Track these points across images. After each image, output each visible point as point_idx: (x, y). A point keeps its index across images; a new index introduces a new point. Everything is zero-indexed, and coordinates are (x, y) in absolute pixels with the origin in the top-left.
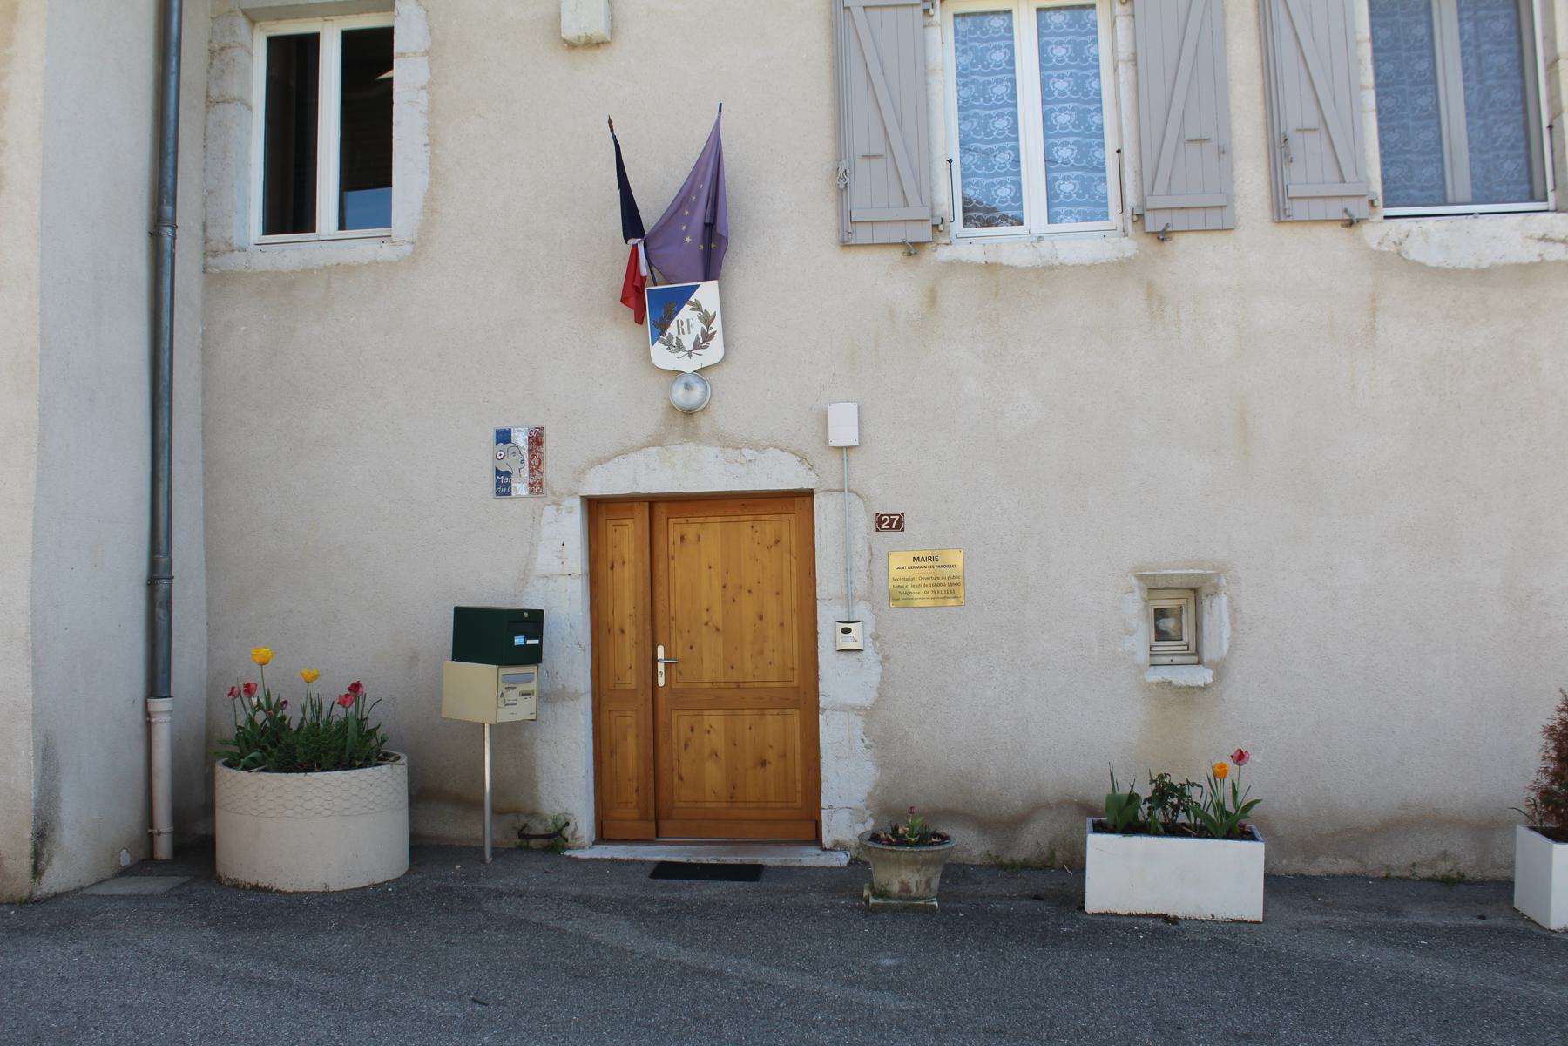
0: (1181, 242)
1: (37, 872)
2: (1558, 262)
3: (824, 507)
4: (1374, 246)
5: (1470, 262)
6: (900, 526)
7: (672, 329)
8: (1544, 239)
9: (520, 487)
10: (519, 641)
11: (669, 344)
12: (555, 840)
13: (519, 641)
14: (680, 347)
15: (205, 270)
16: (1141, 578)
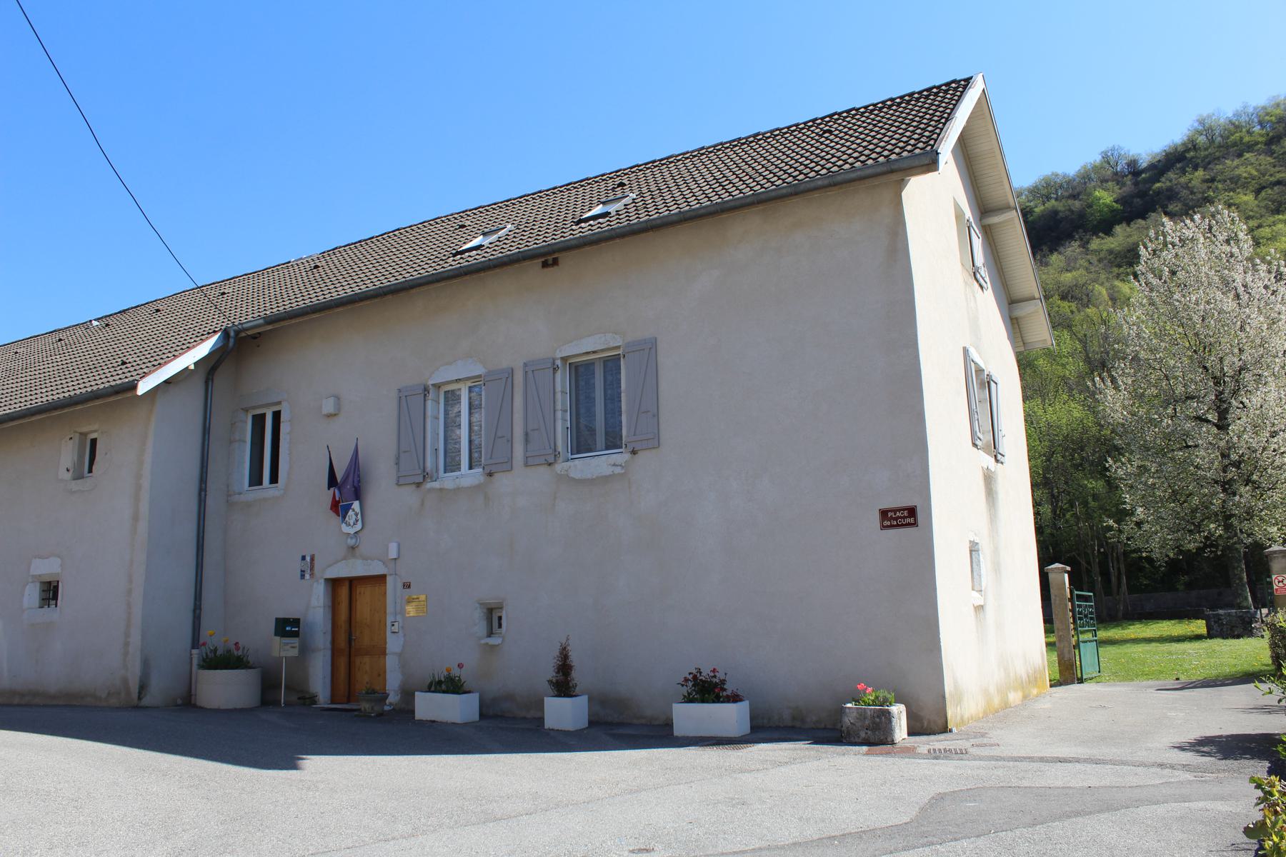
0: (496, 476)
1: (140, 698)
2: (619, 474)
3: (389, 579)
4: (559, 472)
5: (589, 476)
6: (409, 587)
7: (347, 519)
8: (614, 465)
9: (307, 576)
10: (287, 629)
11: (346, 523)
12: (312, 700)
13: (287, 629)
14: (350, 525)
15: (227, 501)
16: (481, 604)
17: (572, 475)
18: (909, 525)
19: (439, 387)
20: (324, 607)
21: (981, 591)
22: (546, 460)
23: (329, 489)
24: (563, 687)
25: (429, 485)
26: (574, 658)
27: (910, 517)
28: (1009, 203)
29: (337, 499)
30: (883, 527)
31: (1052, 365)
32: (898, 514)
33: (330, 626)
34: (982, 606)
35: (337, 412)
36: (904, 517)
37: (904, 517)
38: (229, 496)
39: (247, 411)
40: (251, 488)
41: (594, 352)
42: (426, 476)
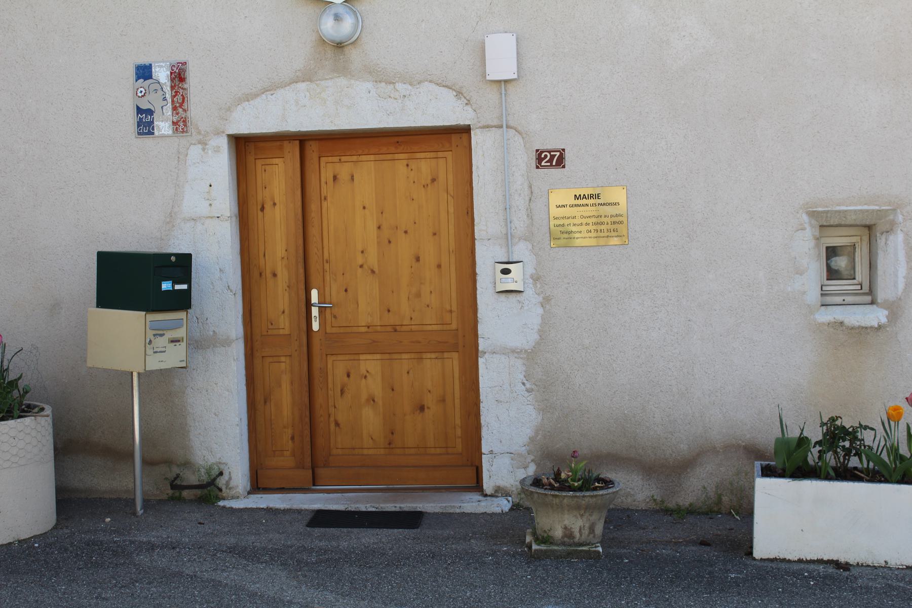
9: (163, 126)
13: (166, 286)
16: (812, 214)
22: (834, 318)
31: (365, 546)
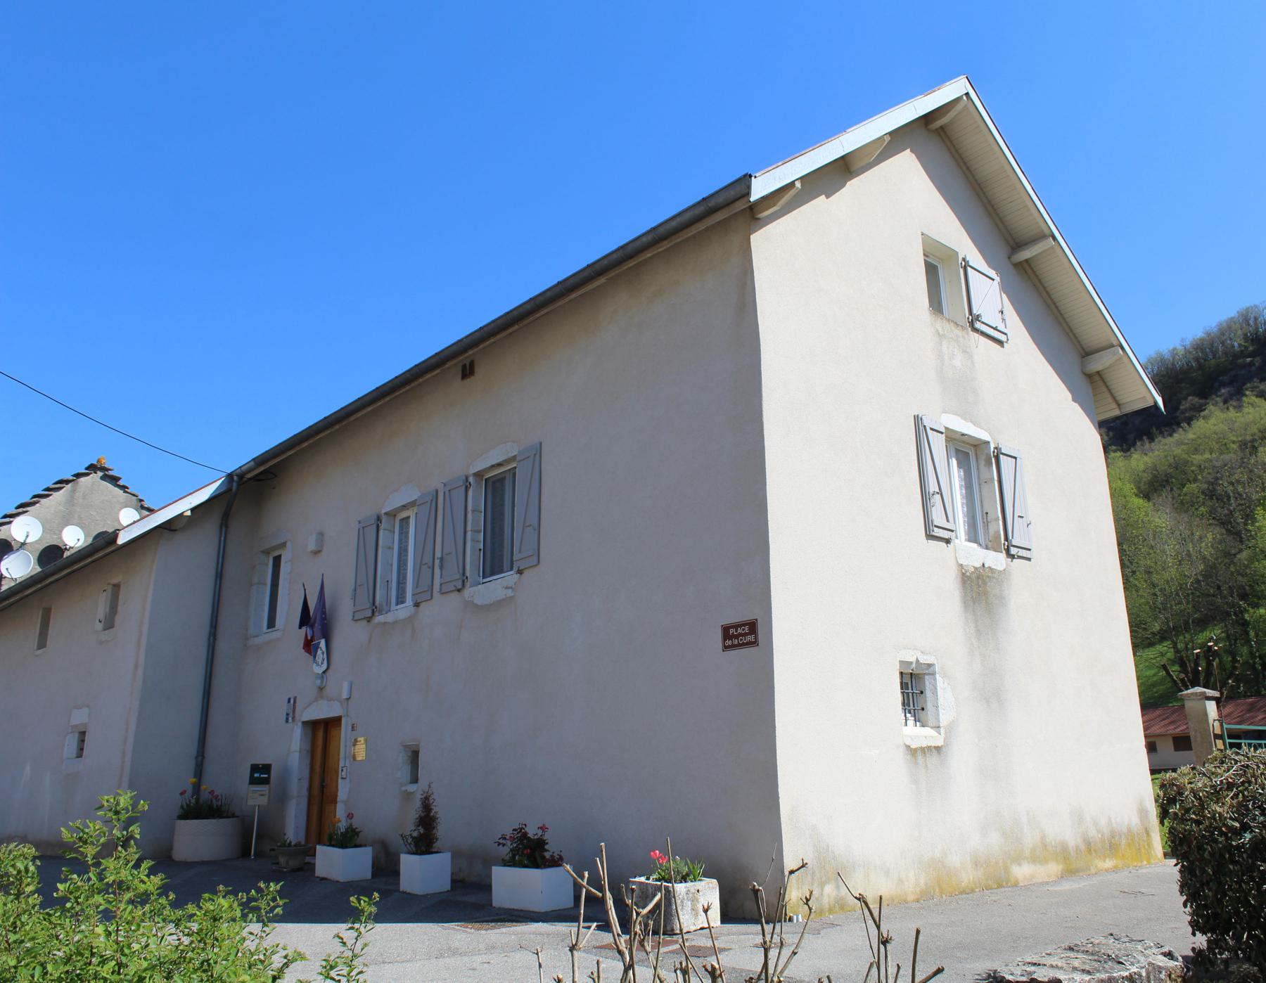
0: (422, 605)
17: (475, 602)
18: (750, 644)
19: (395, 515)
20: (300, 752)
21: (939, 727)
23: (300, 628)
24: (424, 843)
25: (379, 619)
26: (439, 809)
27: (750, 634)
28: (1043, 231)
29: (309, 638)
30: (726, 648)
32: (740, 631)
33: (307, 772)
34: (938, 749)
35: (319, 549)
36: (745, 635)
37: (745, 635)
38: (247, 639)
39: (269, 553)
40: (269, 630)
41: (499, 465)
42: (375, 609)
